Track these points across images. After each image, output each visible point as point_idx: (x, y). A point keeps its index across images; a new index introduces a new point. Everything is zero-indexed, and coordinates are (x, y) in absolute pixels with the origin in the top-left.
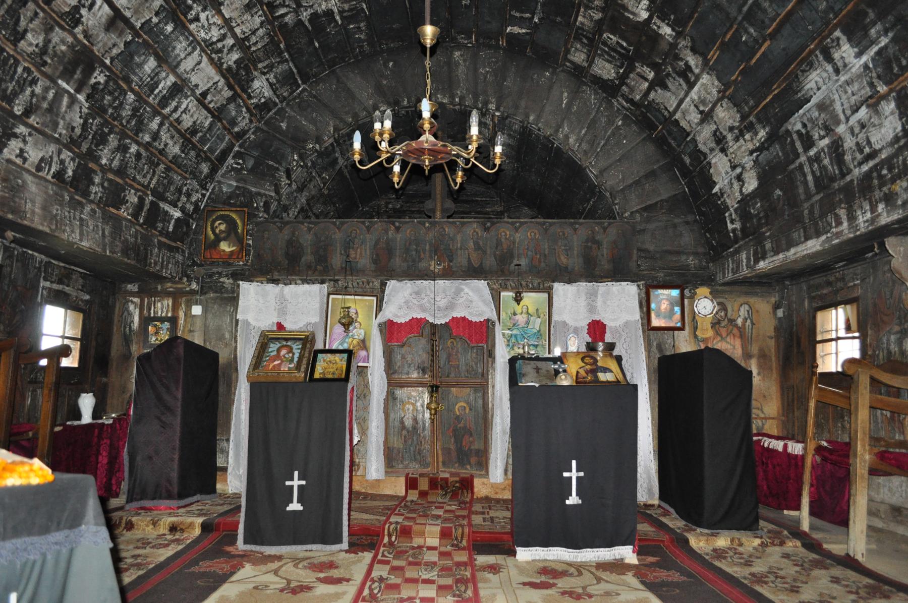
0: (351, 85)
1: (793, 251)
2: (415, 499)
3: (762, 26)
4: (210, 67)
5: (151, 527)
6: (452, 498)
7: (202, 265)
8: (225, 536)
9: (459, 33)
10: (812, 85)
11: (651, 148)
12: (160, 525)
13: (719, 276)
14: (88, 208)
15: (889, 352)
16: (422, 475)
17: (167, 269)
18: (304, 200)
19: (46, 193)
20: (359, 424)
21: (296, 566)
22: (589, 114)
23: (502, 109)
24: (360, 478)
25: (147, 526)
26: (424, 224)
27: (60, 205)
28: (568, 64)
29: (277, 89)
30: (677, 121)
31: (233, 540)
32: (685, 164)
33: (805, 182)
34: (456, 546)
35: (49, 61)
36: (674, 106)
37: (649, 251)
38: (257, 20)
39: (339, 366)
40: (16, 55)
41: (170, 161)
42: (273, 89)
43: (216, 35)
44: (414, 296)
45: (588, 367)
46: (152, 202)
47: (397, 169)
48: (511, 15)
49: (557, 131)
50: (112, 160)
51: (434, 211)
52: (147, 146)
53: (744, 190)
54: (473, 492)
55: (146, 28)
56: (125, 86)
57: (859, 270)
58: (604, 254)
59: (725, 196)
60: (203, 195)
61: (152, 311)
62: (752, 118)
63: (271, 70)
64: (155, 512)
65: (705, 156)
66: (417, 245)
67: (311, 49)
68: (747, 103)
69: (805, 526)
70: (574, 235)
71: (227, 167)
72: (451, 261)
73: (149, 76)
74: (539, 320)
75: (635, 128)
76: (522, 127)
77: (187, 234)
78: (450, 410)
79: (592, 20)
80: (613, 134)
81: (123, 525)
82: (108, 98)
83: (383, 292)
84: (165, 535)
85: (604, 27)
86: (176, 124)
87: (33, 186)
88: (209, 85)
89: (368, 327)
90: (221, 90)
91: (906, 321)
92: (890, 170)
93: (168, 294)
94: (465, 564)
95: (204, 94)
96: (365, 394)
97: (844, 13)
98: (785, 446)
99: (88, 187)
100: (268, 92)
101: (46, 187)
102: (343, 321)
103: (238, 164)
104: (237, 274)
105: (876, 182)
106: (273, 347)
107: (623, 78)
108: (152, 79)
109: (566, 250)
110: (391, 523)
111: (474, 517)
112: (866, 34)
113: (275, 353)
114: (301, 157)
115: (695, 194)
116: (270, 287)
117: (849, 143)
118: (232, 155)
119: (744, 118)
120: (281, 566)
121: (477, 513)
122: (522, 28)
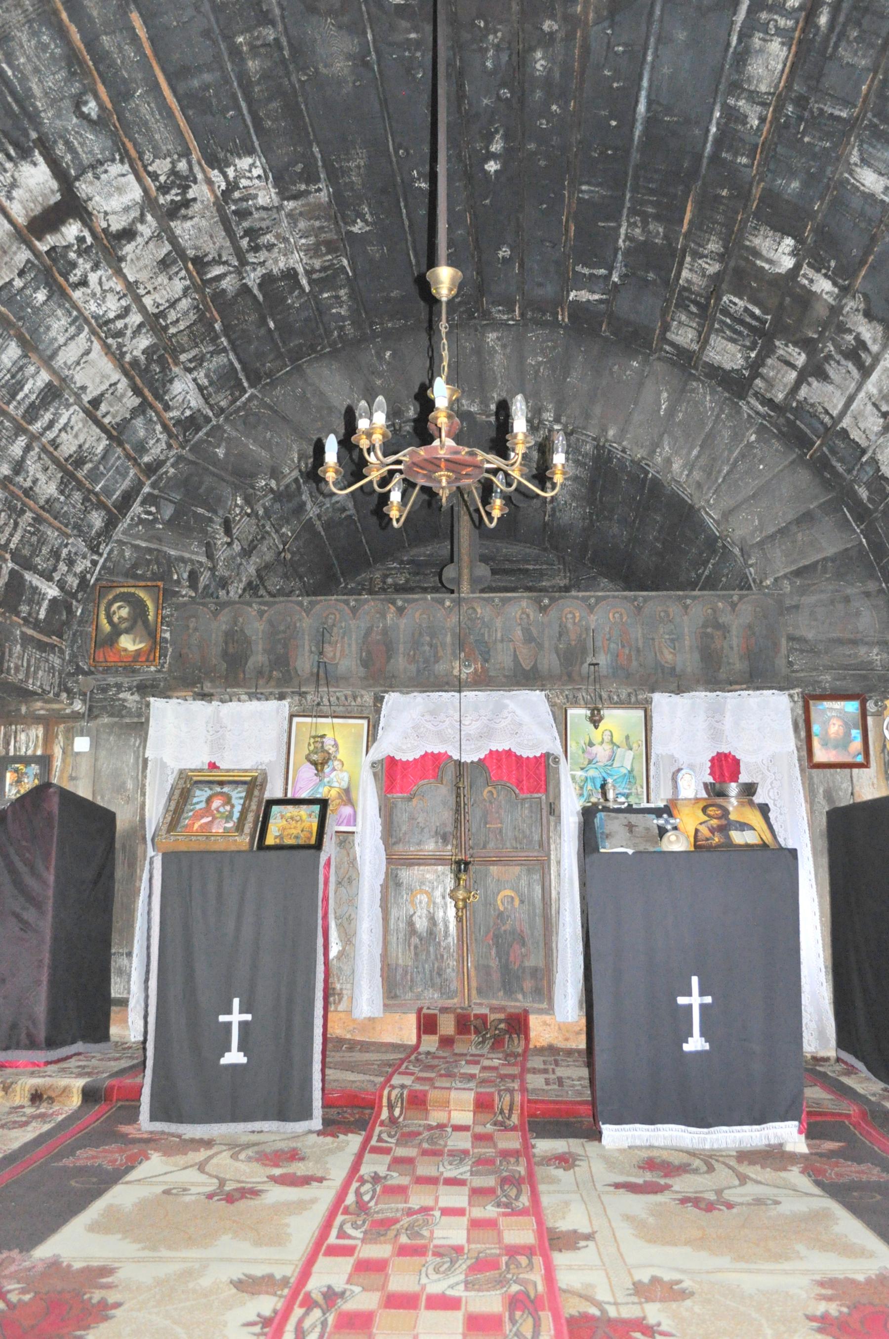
2: (433, 1050)
4: (105, 359)
6: (493, 1048)
9: (495, 303)
11: (804, 476)
12: (14, 1091)
16: (444, 1010)
18: (252, 570)
20: (339, 926)
21: (234, 1157)
24: (342, 1015)
26: (441, 602)
28: (667, 348)
29: (210, 395)
30: (844, 431)
31: (133, 1116)
32: (861, 500)
34: (502, 1124)
37: (806, 641)
38: (178, 286)
39: (306, 824)
41: (42, 508)
42: (203, 395)
43: (114, 308)
44: (428, 717)
45: (714, 822)
46: (12, 572)
47: (396, 497)
48: (575, 273)
51: (458, 581)
54: (527, 1039)
58: (733, 648)
60: (94, 563)
61: (12, 747)
63: (201, 365)
64: (9, 1070)
66: (433, 635)
67: (263, 331)
71: (132, 519)
72: (486, 661)
73: (9, 371)
74: (630, 754)
75: (776, 444)
76: (597, 447)
77: (67, 623)
78: (488, 903)
79: (704, 276)
80: (743, 456)
83: (378, 711)
84: (23, 1107)
85: (724, 286)
86: (51, 449)
88: (104, 387)
89: (353, 770)
90: (123, 395)
93: (38, 720)
94: (516, 1154)
95: (96, 402)
96: (350, 878)
100: (195, 401)
102: (315, 757)
103: (149, 513)
104: (146, 687)
106: (200, 795)
107: (755, 367)
108: (13, 377)
109: (672, 640)
111: (529, 1077)
114: (248, 501)
116: (199, 706)
118: (139, 499)
120: (210, 1157)
121: (534, 1071)
122: (594, 292)
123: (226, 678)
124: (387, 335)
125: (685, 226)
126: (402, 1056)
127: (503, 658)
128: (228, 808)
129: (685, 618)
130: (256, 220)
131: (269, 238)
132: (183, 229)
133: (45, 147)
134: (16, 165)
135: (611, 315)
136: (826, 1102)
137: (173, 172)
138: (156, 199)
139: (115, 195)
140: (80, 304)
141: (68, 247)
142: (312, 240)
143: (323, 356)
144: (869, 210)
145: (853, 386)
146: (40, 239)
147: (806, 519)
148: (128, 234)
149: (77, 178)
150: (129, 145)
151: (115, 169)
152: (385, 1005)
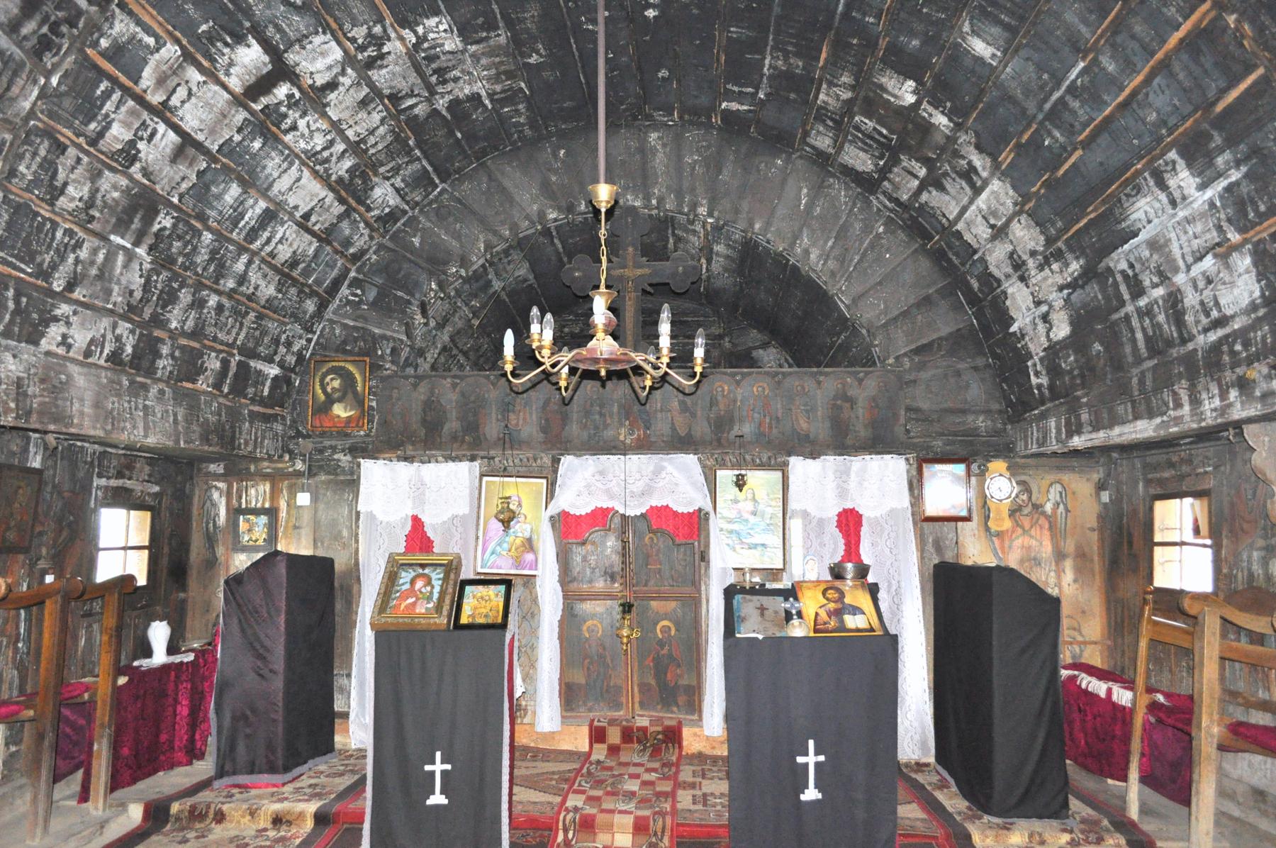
0: (507, 183)
1: (1117, 430)
2: (602, 758)
3: (1071, 131)
5: (248, 817)
7: (308, 436)
8: (347, 829)
10: (1140, 215)
11: (925, 264)
13: (1020, 446)
14: (154, 391)
15: (1251, 575)
16: (612, 722)
17: (262, 447)
18: (446, 338)
19: (98, 384)
22: (839, 218)
23: (716, 214)
24: (527, 727)
25: (243, 817)
27: (119, 395)
33: (1134, 341)
35: (97, 215)
36: (955, 214)
38: (376, 117)
39: (494, 603)
40: (53, 217)
41: (264, 307)
44: (597, 477)
45: (832, 606)
46: (240, 363)
49: (793, 244)
50: (184, 322)
52: (231, 294)
53: (1052, 335)
54: (681, 747)
55: (225, 149)
56: (198, 225)
57: (1211, 453)
58: (860, 417)
59: (1027, 338)
61: (243, 500)
62: (1060, 244)
65: (999, 281)
66: (602, 406)
68: (1053, 224)
69: (1134, 812)
70: (821, 387)
75: (902, 235)
77: (288, 394)
79: (838, 99)
80: (872, 246)
81: (211, 815)
82: (177, 244)
83: (555, 471)
84: (265, 830)
87: (80, 378)
88: (313, 204)
89: (536, 521)
90: (330, 207)
91: (1273, 536)
92: (1246, 345)
93: (265, 477)
95: (307, 216)
97: (1181, 130)
98: (1109, 691)
99: (153, 362)
100: (393, 200)
101: (99, 377)
102: (502, 517)
103: (356, 295)
105: (1226, 358)
106: (405, 577)
108: (235, 211)
109: (807, 411)
110: (567, 810)
112: (1211, 163)
113: (407, 586)
114: (441, 286)
115: (985, 328)
117: (1191, 299)
118: (346, 283)
119: (1050, 241)
123: (425, 442)
124: (562, 135)
125: (821, 63)
126: (577, 766)
127: (661, 426)
128: (429, 588)
129: (818, 392)
130: (443, 61)
131: (456, 73)
132: (380, 76)
133: (258, 33)
134: (232, 49)
135: (758, 122)
136: (918, 824)
137: (370, 35)
138: (355, 56)
139: (319, 59)
140: (292, 145)
141: (280, 103)
142: (493, 71)
143: (504, 153)
144: (978, 69)
145: (965, 200)
146: (255, 101)
147: (926, 302)
148: (332, 85)
149: (286, 51)
150: (331, 20)
151: (318, 40)
152: (563, 717)
